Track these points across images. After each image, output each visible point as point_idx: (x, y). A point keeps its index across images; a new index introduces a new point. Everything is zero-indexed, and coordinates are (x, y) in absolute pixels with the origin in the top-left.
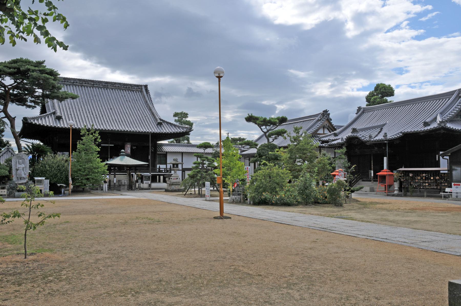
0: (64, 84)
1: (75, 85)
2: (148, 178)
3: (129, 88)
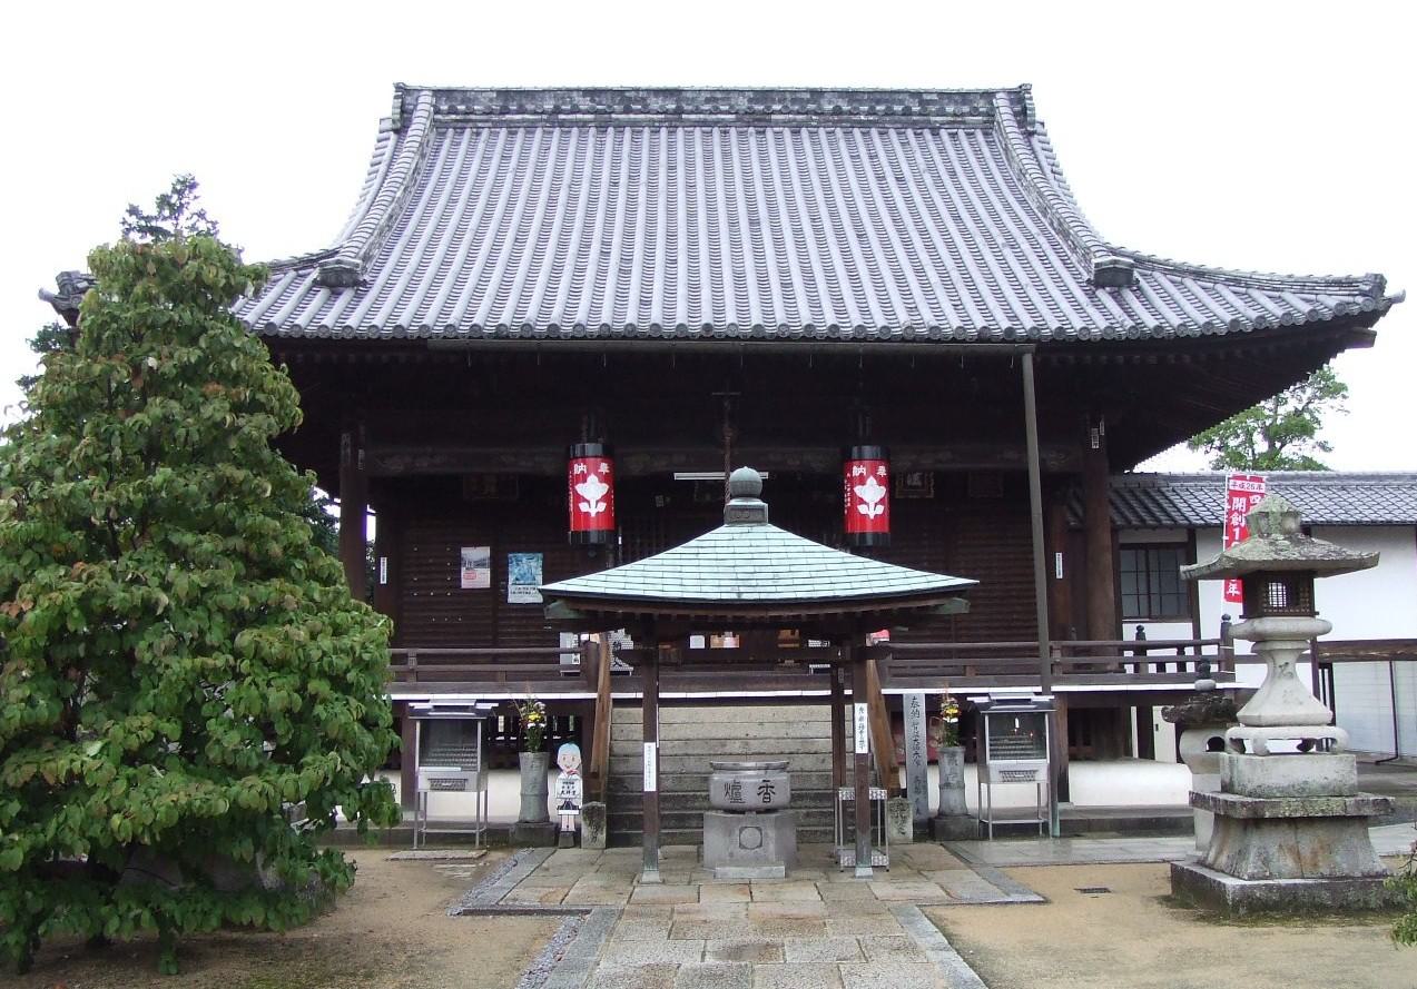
0: (498, 125)
1: (562, 124)
2: (1023, 730)
3: (907, 112)
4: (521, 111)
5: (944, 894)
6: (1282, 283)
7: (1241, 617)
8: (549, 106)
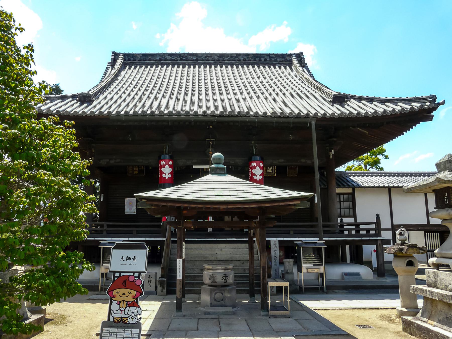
4: (150, 60)
5: (301, 327)
6: (398, 100)
7: (435, 208)
8: (158, 59)
